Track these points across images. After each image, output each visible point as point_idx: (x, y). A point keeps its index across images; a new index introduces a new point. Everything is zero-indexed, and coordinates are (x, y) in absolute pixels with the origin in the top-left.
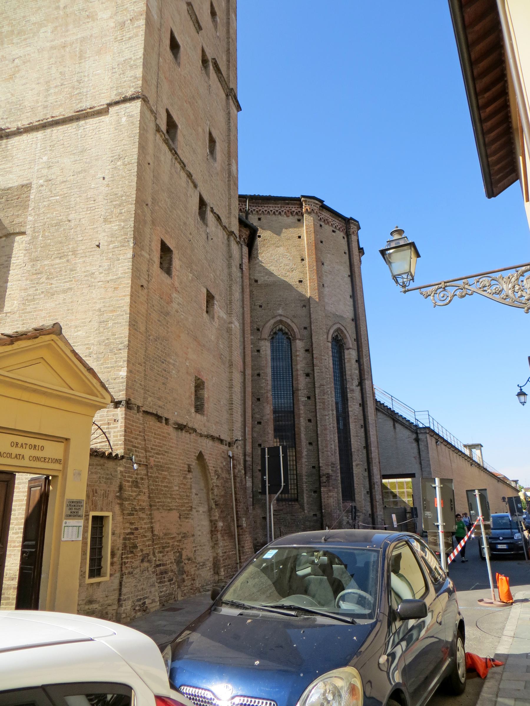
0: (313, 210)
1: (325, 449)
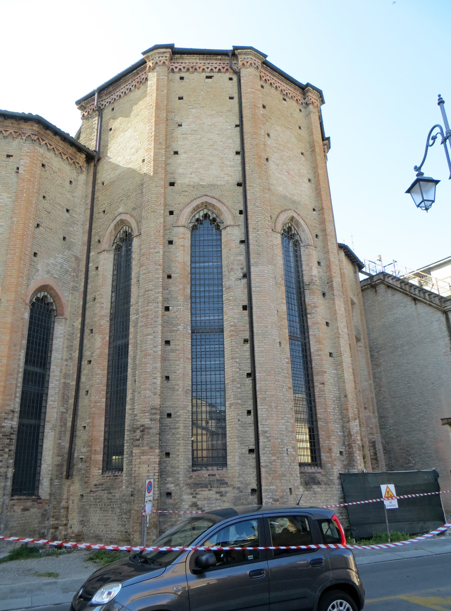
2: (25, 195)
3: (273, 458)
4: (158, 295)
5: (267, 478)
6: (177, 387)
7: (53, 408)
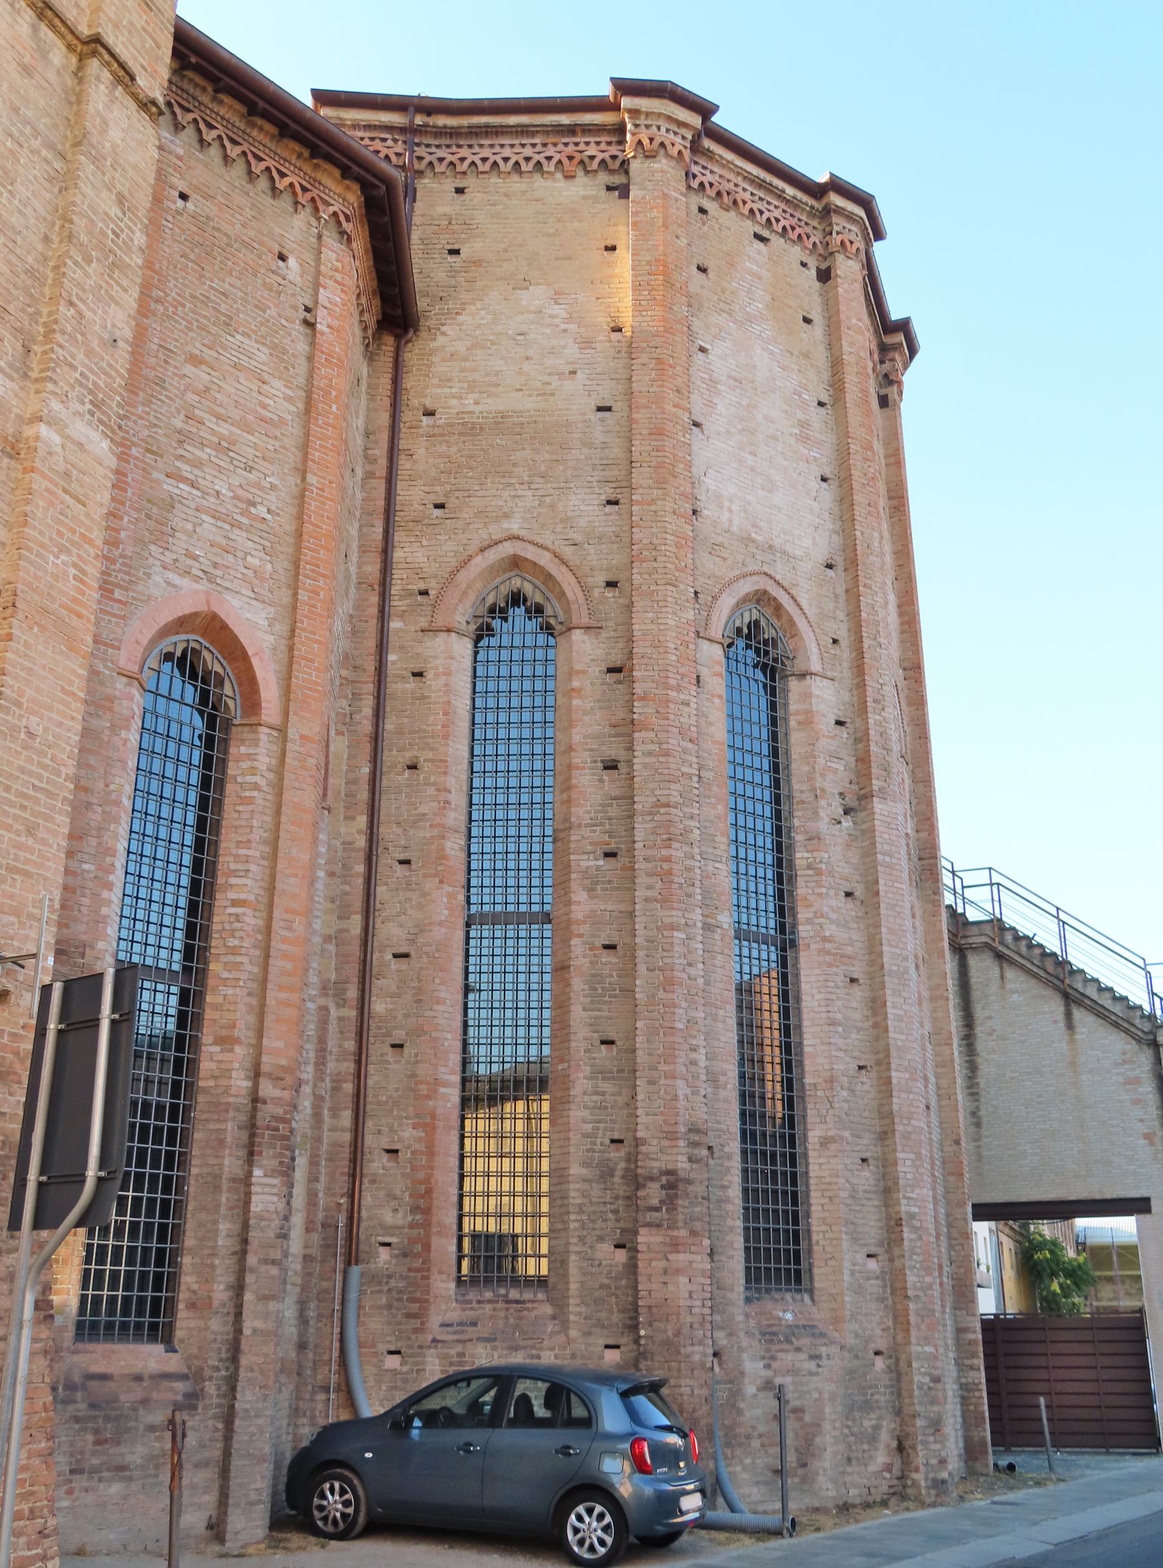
0: (662, 145)
2: (334, 408)
5: (919, 1329)
6: (722, 1079)
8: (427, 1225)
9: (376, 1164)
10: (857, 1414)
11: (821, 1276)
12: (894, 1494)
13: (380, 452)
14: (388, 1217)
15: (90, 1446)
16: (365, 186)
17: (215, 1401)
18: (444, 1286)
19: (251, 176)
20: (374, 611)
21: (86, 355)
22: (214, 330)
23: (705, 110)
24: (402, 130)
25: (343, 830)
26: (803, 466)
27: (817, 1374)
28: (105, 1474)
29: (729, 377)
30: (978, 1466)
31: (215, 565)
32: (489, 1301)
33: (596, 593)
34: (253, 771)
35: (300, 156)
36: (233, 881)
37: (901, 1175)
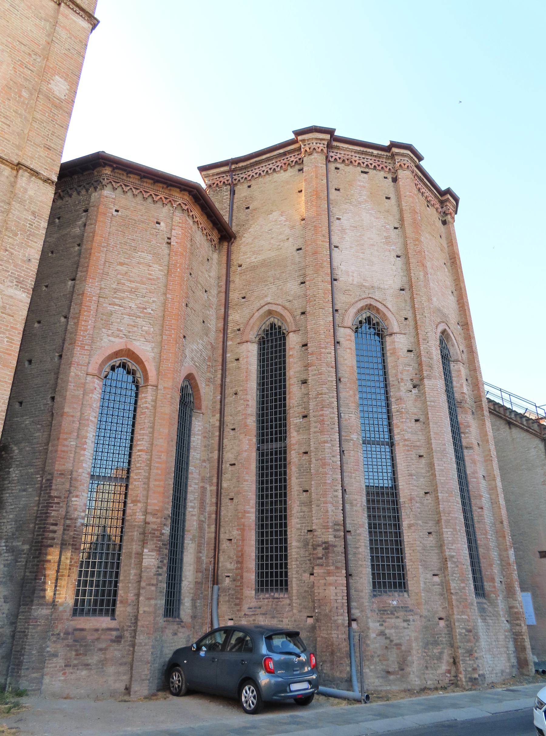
0: (314, 149)
1: (322, 499)
3: (462, 585)
4: (333, 400)
6: (355, 502)
7: (193, 515)
8: (241, 568)
9: (224, 545)
10: (430, 647)
11: (411, 584)
12: (452, 684)
13: (223, 283)
14: (229, 566)
15: (73, 656)
16: (190, 192)
17: (129, 639)
18: (250, 592)
19: (145, 199)
20: (221, 340)
21: (14, 266)
22: (129, 252)
23: (330, 132)
24: (228, 172)
25: (211, 421)
26: (387, 253)
27: (408, 628)
28: (80, 667)
29: (351, 226)
30: (525, 671)
31: (129, 332)
32: (267, 598)
33: (298, 318)
34: (146, 402)
35: (163, 188)
36: (139, 443)
37: (446, 539)
